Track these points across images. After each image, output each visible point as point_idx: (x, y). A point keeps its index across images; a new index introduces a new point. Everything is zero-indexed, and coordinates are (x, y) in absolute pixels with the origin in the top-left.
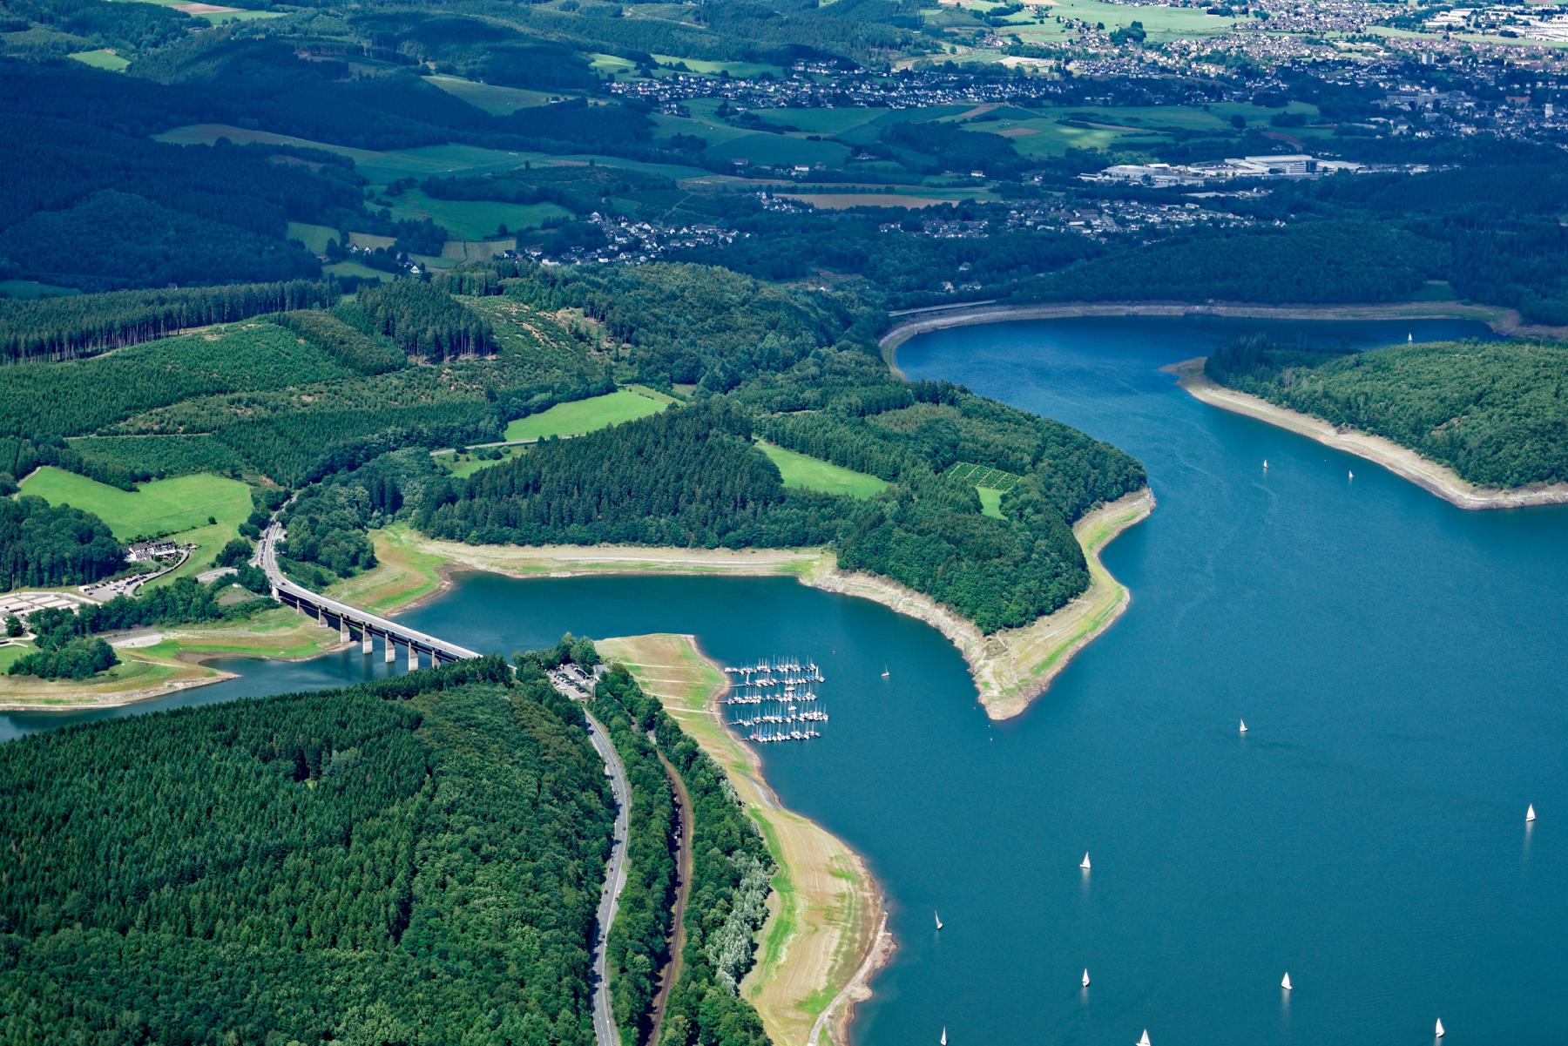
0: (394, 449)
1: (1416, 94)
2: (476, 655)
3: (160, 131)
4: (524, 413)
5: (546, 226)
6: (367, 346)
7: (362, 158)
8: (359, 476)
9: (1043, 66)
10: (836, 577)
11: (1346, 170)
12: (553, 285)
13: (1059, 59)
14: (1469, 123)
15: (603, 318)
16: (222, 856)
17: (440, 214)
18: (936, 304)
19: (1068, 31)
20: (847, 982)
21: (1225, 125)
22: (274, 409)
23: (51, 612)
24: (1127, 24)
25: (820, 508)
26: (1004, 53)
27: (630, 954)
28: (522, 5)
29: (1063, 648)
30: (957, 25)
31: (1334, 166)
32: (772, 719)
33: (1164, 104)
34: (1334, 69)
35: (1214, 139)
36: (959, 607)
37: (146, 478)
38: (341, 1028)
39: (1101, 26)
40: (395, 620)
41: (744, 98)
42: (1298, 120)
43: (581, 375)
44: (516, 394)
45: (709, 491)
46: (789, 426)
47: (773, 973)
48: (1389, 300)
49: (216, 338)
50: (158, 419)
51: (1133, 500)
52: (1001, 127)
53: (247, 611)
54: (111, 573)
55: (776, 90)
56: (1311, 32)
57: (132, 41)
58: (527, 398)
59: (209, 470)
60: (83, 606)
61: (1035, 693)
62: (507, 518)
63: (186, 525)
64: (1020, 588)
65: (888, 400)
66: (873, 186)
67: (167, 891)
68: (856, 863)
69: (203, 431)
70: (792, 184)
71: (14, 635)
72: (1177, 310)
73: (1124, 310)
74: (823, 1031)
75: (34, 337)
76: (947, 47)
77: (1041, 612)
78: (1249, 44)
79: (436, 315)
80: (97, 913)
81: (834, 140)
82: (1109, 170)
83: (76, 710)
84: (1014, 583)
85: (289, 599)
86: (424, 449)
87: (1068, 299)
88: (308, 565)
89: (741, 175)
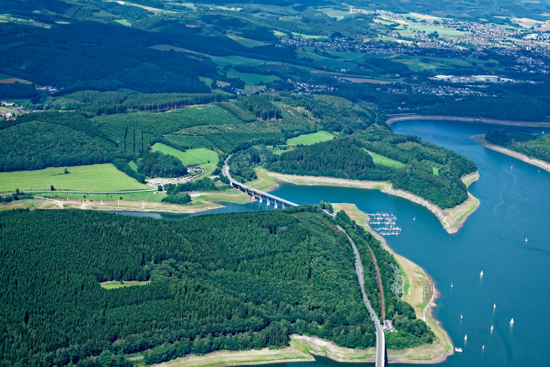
0: (256, 145)
1: (526, 59)
2: (298, 205)
3: (151, 46)
4: (291, 137)
5: (274, 82)
6: (247, 115)
7: (214, 58)
8: (248, 152)
9: (410, 43)
10: (392, 190)
11: (510, 81)
12: (295, 99)
13: (414, 41)
14: (543, 69)
15: (311, 110)
16: (259, 253)
19: (414, 33)
21: (471, 65)
22: (221, 131)
23: (170, 185)
24: (433, 32)
26: (397, 38)
27: (372, 288)
28: (343, 4)
29: (464, 215)
30: (380, 29)
31: (506, 80)
32: (385, 229)
33: (451, 57)
34: (500, 50)
35: (468, 69)
36: (432, 201)
37: (188, 148)
38: (301, 302)
39: (424, 32)
41: (322, 47)
42: (493, 65)
43: (307, 127)
44: (289, 131)
46: (374, 145)
47: (408, 297)
48: (536, 121)
49: (200, 109)
50: (188, 131)
51: (474, 174)
52: (403, 61)
53: (224, 189)
54: (183, 175)
55: (330, 46)
56: (490, 38)
57: (131, 17)
59: (204, 147)
60: (178, 184)
61: (459, 227)
64: (451, 197)
65: (400, 140)
67: (245, 262)
68: (421, 270)
70: (342, 74)
72: (471, 120)
73: (455, 119)
74: (426, 314)
75: (149, 105)
76: (380, 36)
77: (457, 204)
78: (471, 40)
79: (265, 106)
81: (352, 62)
82: (437, 76)
83: (182, 213)
85: (236, 186)
86: (264, 145)
87: (438, 114)
88: (238, 176)
89: (325, 71)
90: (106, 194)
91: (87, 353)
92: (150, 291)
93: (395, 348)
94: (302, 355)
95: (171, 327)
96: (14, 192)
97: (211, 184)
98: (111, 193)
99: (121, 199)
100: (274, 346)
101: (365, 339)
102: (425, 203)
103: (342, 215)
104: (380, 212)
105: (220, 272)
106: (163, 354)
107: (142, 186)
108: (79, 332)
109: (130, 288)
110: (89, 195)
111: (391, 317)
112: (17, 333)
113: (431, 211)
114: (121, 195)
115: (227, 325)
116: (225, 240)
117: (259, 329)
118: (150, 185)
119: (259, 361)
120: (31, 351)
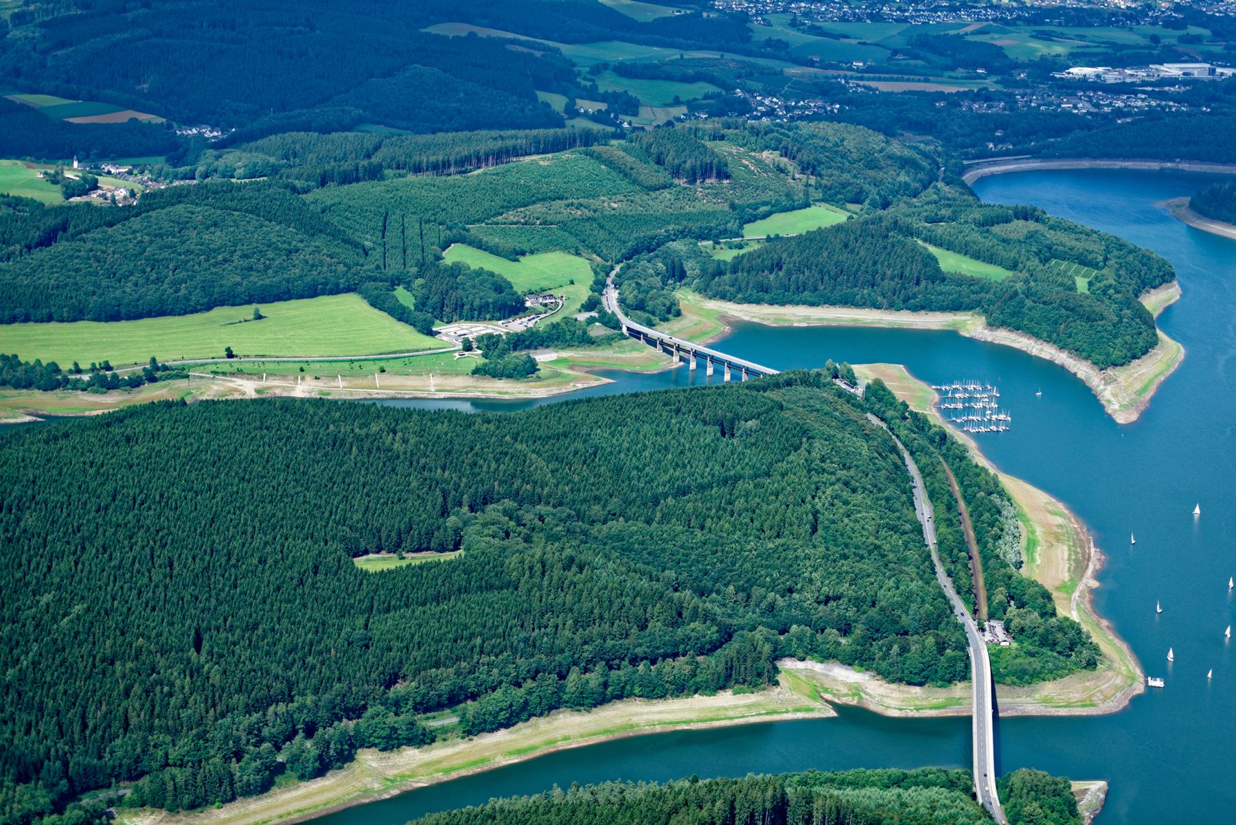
0: (674, 240)
4: (753, 219)
5: (706, 97)
6: (649, 173)
7: (566, 49)
8: (657, 256)
12: (757, 135)
15: (794, 158)
16: (700, 480)
17: (633, 88)
18: (991, 157)
20: (1082, 576)
21: (1143, 41)
23: (490, 336)
25: (970, 286)
29: (1151, 381)
32: (974, 418)
35: (1140, 51)
36: (1077, 352)
37: (523, 253)
38: (799, 586)
41: (807, 14)
42: (1198, 39)
44: (748, 206)
45: (896, 272)
50: (523, 215)
51: (1168, 288)
52: (992, 39)
53: (609, 341)
54: (516, 314)
58: (755, 210)
60: (508, 333)
61: (1142, 408)
62: (762, 287)
63: (556, 286)
66: (917, 78)
67: (670, 501)
69: (552, 224)
71: (468, 350)
72: (1155, 165)
73: (1118, 164)
75: (433, 159)
77: (1134, 357)
80: (629, 513)
82: (1071, 70)
84: (1116, 337)
85: (635, 334)
89: (818, 67)
92: (465, 572)
93: (1014, 683)
94: (807, 703)
95: (515, 650)
96: (145, 364)
97: (579, 333)
98: (360, 360)
99: (383, 371)
100: (745, 687)
102: (1062, 358)
103: (877, 391)
104: (961, 380)
105: (616, 525)
106: (501, 710)
107: (427, 341)
108: (313, 668)
109: (421, 567)
112: (179, 674)
113: (1075, 374)
114: (382, 364)
115: (637, 643)
116: (622, 456)
117: (714, 647)
118: (445, 338)
119: (712, 720)
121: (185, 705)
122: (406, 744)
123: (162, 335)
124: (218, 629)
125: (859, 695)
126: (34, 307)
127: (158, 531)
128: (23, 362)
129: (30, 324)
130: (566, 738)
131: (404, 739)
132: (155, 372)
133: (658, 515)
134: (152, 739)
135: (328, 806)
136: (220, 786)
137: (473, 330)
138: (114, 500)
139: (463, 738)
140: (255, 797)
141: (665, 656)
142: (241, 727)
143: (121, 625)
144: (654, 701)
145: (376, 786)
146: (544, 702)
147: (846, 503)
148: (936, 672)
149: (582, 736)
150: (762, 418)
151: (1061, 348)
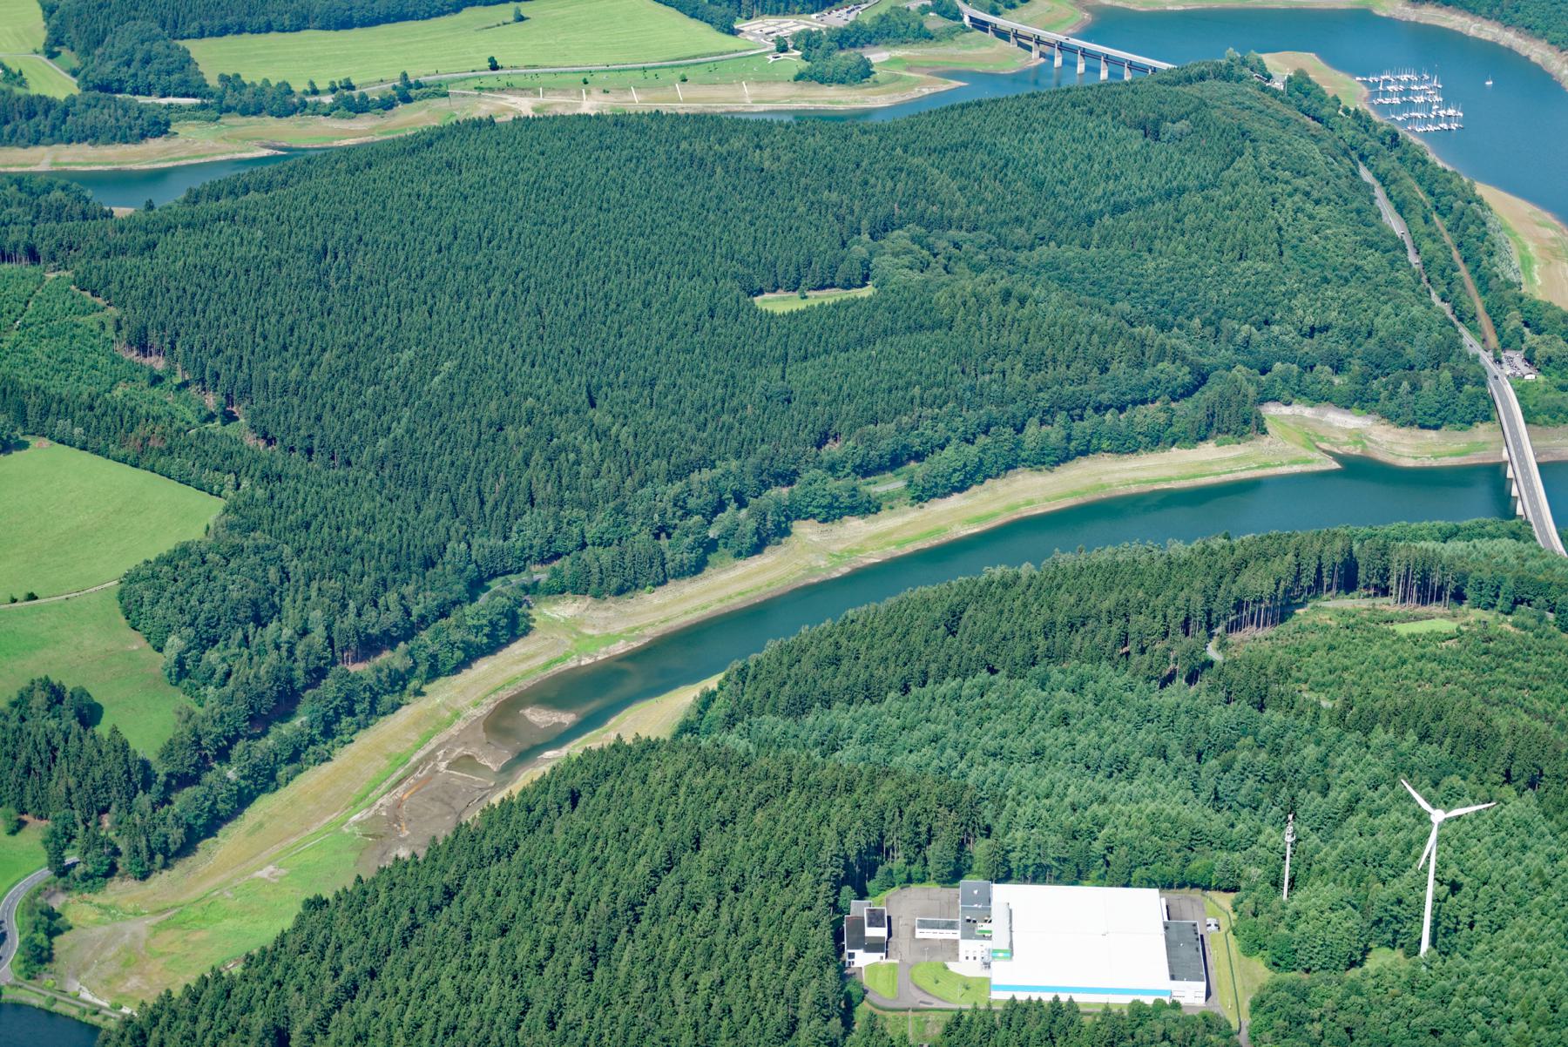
16: (1138, 194)
36: (1529, 29)
38: (1277, 317)
40: (1074, 36)
53: (950, 34)
68: (1548, 217)
85: (981, 25)
90: (640, 69)
91: (762, 481)
92: (889, 310)
93: (1546, 423)
94: (1304, 454)
95: (960, 401)
96: (393, 81)
97: (914, 25)
98: (654, 68)
99: (685, 80)
100: (1229, 437)
101: (1466, 404)
102: (1508, 38)
103: (1300, 86)
104: (1392, 70)
105: (1045, 252)
106: (955, 471)
107: (729, 42)
108: (731, 428)
109: (836, 306)
110: (596, 76)
111: (1517, 342)
112: (585, 438)
113: (1527, 58)
114: (682, 72)
115: (1097, 388)
116: (1040, 167)
117: (1188, 392)
118: (751, 38)
119: (1195, 476)
120: (629, 482)
121: (597, 475)
122: (848, 514)
123: (405, 44)
124: (610, 385)
125: (1362, 442)
126: (248, 14)
127: (517, 274)
128: (247, 83)
129: (246, 35)
130: (1030, 503)
131: (846, 507)
132: (406, 92)
133: (1096, 236)
134: (567, 513)
135: (772, 588)
136: (651, 567)
137: (782, 26)
138: (456, 238)
139: (912, 505)
140: (688, 579)
141: (1135, 403)
142: (666, 498)
143: (502, 384)
144: (1126, 457)
145: (822, 563)
146: (1001, 461)
147: (1311, 217)
148: (1455, 412)
149: (1047, 500)
150: (1192, 116)
151: (1507, 26)
